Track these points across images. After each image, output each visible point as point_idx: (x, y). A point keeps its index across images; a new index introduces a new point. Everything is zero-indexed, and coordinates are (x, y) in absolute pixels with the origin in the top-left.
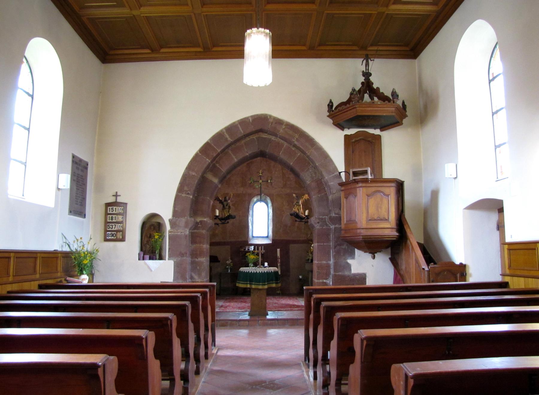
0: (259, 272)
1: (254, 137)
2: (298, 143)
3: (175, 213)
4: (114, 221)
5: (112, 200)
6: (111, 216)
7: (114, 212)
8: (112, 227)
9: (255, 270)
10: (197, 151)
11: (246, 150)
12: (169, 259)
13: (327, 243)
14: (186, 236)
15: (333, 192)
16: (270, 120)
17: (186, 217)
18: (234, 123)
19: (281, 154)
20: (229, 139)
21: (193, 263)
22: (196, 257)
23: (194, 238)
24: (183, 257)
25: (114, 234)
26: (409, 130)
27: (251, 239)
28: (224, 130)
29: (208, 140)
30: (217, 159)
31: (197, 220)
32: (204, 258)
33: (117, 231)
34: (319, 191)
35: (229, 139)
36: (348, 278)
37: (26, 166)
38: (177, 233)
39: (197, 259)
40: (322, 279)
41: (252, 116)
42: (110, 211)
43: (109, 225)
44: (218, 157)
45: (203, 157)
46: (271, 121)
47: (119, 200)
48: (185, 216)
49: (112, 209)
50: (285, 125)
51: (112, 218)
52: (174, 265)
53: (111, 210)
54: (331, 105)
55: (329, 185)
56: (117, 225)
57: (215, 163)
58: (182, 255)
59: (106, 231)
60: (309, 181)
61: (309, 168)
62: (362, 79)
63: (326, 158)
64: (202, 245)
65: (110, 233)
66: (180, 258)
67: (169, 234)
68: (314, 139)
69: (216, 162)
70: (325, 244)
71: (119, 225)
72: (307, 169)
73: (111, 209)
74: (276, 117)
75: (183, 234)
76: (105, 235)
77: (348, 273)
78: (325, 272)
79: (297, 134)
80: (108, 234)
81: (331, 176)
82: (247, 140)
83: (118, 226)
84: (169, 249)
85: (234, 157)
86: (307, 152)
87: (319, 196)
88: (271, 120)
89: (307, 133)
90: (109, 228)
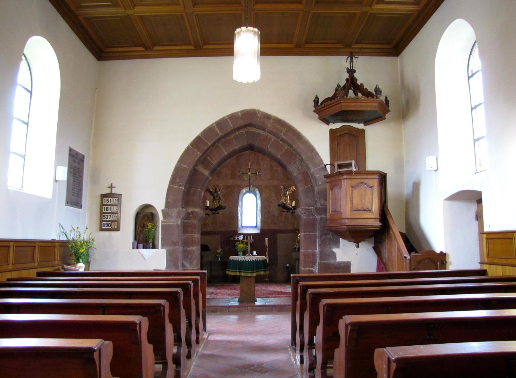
0: (248, 260)
2: (285, 137)
3: (168, 204)
4: (109, 211)
5: (107, 191)
6: (106, 207)
7: (109, 203)
8: (107, 217)
9: (244, 258)
10: (189, 145)
11: (235, 143)
12: (161, 248)
13: (313, 233)
14: (178, 226)
15: (319, 183)
16: (258, 115)
17: (178, 208)
18: (224, 118)
19: (269, 147)
20: (219, 133)
21: (184, 251)
22: (188, 246)
23: (186, 228)
24: (175, 246)
25: (109, 223)
26: (392, 124)
27: (240, 229)
28: (215, 124)
29: (199, 134)
30: (208, 152)
31: (189, 210)
32: (195, 247)
33: (112, 221)
34: (306, 183)
35: (219, 133)
36: (333, 266)
37: (24, 159)
38: (169, 223)
39: (189, 248)
40: (308, 267)
41: (241, 111)
42: (105, 202)
43: (104, 215)
44: (209, 150)
45: (195, 150)
46: (260, 116)
47: (114, 191)
48: (177, 207)
49: (107, 200)
50: (273, 120)
51: (107, 208)
52: (167, 254)
53: (106, 201)
54: (317, 100)
55: (315, 177)
56: (112, 215)
57: (206, 156)
58: (174, 244)
59: (101, 221)
60: (296, 173)
61: (296, 161)
62: (347, 76)
63: (312, 151)
64: (193, 234)
65: (105, 223)
66: (172, 247)
67: (161, 224)
68: (300, 133)
69: (207, 155)
70: (311, 233)
71: (114, 215)
73: (106, 200)
74: (264, 112)
75: (175, 224)
76: (101, 225)
77: (333, 261)
78: (311, 260)
79: (284, 128)
80: (104, 223)
81: (317, 168)
82: (236, 134)
83: (113, 217)
84: (162, 238)
85: (224, 150)
86: (294, 146)
87: (306, 187)
88: (259, 115)
89: (294, 127)
90: (104, 219)
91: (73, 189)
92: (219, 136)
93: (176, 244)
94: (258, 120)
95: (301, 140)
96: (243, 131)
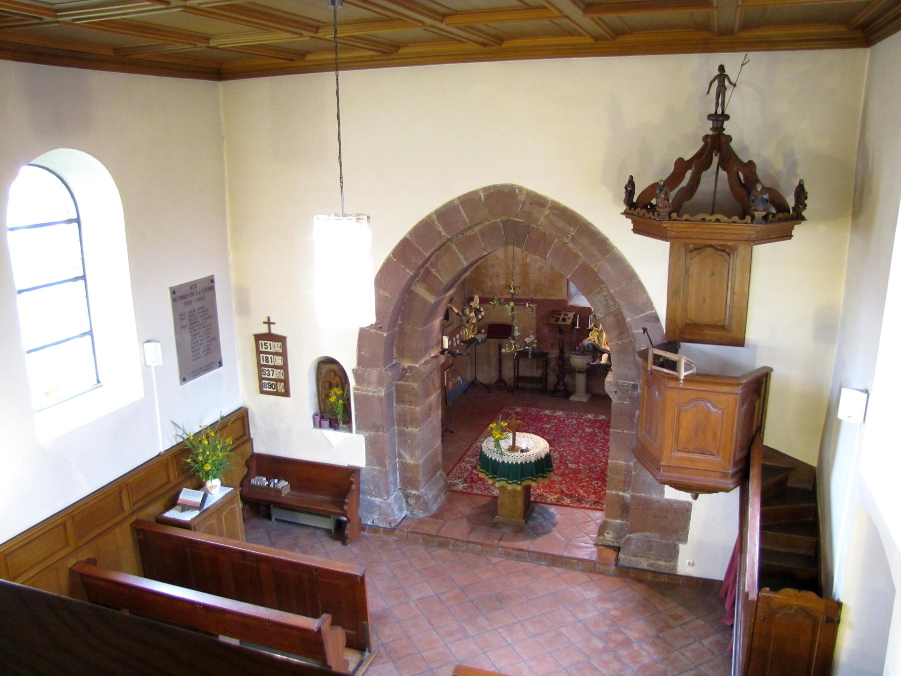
0: (508, 462)
2: (574, 247)
3: (361, 360)
4: (270, 363)
5: (264, 329)
6: (265, 356)
7: (268, 350)
8: (269, 373)
9: (500, 458)
10: (389, 254)
11: (483, 245)
12: (357, 433)
13: (630, 431)
14: (381, 399)
15: (640, 347)
16: (519, 197)
17: (379, 369)
18: (451, 202)
19: (549, 255)
20: (443, 233)
21: (401, 433)
22: (405, 426)
23: (400, 395)
24: (378, 431)
25: (273, 384)
26: (822, 228)
27: (575, 295)
28: (434, 216)
29: (406, 235)
30: (431, 259)
31: (404, 364)
32: (417, 428)
34: (620, 334)
35: (443, 233)
36: (657, 504)
37: (92, 336)
38: (366, 393)
39: (407, 428)
40: (617, 490)
41: (485, 189)
42: (262, 348)
43: (263, 369)
44: (434, 256)
45: (401, 265)
46: (522, 199)
47: (275, 330)
48: (376, 367)
49: (265, 345)
50: (550, 208)
51: (267, 359)
52: (366, 442)
53: (264, 346)
54: (631, 191)
55: (633, 333)
56: (275, 370)
57: (429, 266)
58: (377, 428)
59: (261, 379)
60: (601, 314)
61: (602, 288)
62: (707, 128)
63: (631, 280)
64: (413, 407)
65: (267, 382)
66: (373, 433)
67: (354, 392)
68: (607, 239)
69: (431, 265)
70: (625, 431)
71: (279, 371)
73: (263, 344)
74: (532, 192)
75: (376, 394)
76: (261, 386)
77: (658, 497)
78: (623, 479)
79: (573, 227)
80: (265, 383)
81: (638, 316)
82: (484, 225)
83: (278, 374)
84: (356, 417)
85: (462, 257)
86: (592, 266)
87: (620, 343)
88: (522, 198)
89: (592, 225)
90: (264, 375)
91: (202, 338)
94: (519, 209)
96: (498, 220)
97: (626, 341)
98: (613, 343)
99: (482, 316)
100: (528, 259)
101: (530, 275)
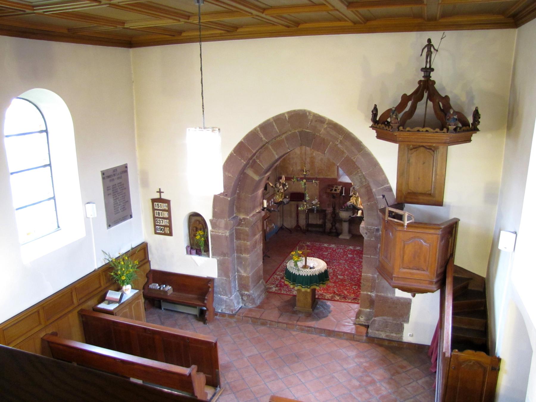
0: (302, 275)
1: (296, 131)
2: (342, 147)
3: (215, 214)
4: (161, 216)
5: (157, 196)
6: (157, 211)
7: (160, 208)
8: (160, 222)
9: (298, 272)
10: (232, 151)
11: (287, 146)
12: (212, 257)
13: (375, 256)
14: (227, 237)
15: (381, 207)
16: (309, 117)
17: (225, 219)
18: (268, 120)
19: (327, 152)
20: (264, 139)
21: (239, 258)
22: (241, 253)
23: (238, 235)
24: (225, 257)
25: (162, 228)
26: (489, 136)
27: (342, 175)
28: (258, 128)
29: (242, 140)
30: (257, 154)
31: (240, 217)
32: (248, 254)
33: (165, 226)
34: (369, 199)
35: (264, 139)
36: (391, 300)
37: (55, 200)
38: (218, 234)
39: (242, 255)
40: (367, 291)
41: (288, 113)
42: (156, 207)
43: (157, 220)
44: (258, 152)
45: (238, 157)
46: (311, 118)
47: (164, 196)
48: (224, 218)
49: (158, 205)
50: (327, 124)
51: (159, 213)
52: (217, 263)
53: (157, 206)
54: (375, 114)
55: (376, 198)
56: (164, 220)
57: (255, 158)
58: (224, 255)
59: (155, 225)
60: (358, 186)
61: (358, 171)
62: (421, 76)
63: (375, 167)
64: (246, 242)
65: (159, 227)
66: (222, 257)
67: (210, 233)
68: (361, 142)
69: (256, 158)
70: (372, 257)
71: (166, 220)
72: (356, 172)
73: (157, 205)
74: (316, 114)
75: (223, 235)
76: (155, 230)
77: (392, 295)
78: (370, 285)
79: (341, 135)
80: (158, 228)
81: (380, 188)
82: (288, 134)
83: (165, 222)
84: (212, 248)
85: (275, 153)
86: (352, 158)
87: (369, 204)
88: (310, 118)
89: (352, 134)
90: (157, 223)
92: (264, 143)
93: (225, 255)
95: (362, 151)
97: (372, 203)
98: (364, 204)
99: (287, 188)
100: (314, 154)
101: (315, 163)
